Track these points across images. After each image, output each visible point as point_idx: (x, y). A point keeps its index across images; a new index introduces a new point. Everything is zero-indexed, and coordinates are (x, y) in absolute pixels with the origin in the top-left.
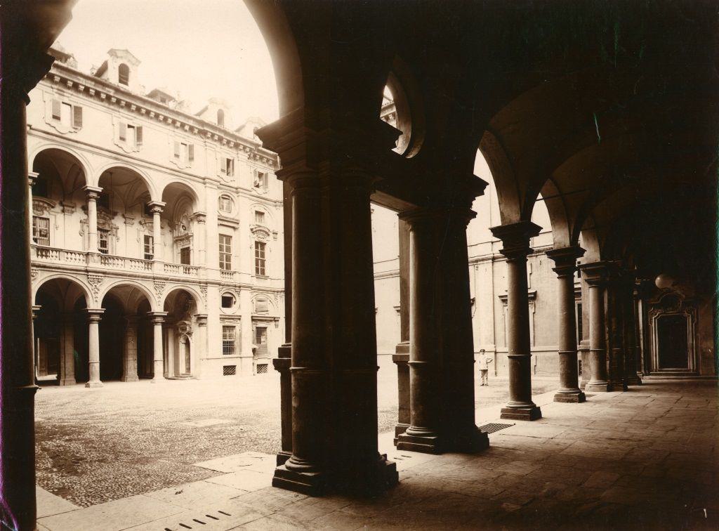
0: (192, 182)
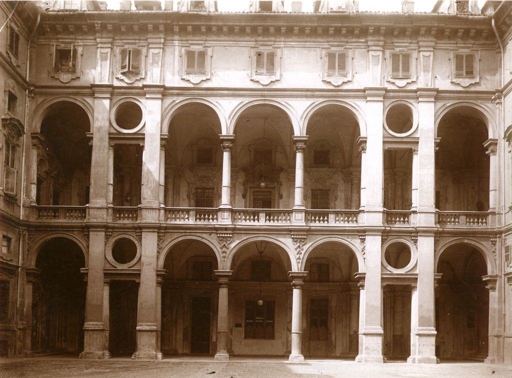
0: (279, 100)
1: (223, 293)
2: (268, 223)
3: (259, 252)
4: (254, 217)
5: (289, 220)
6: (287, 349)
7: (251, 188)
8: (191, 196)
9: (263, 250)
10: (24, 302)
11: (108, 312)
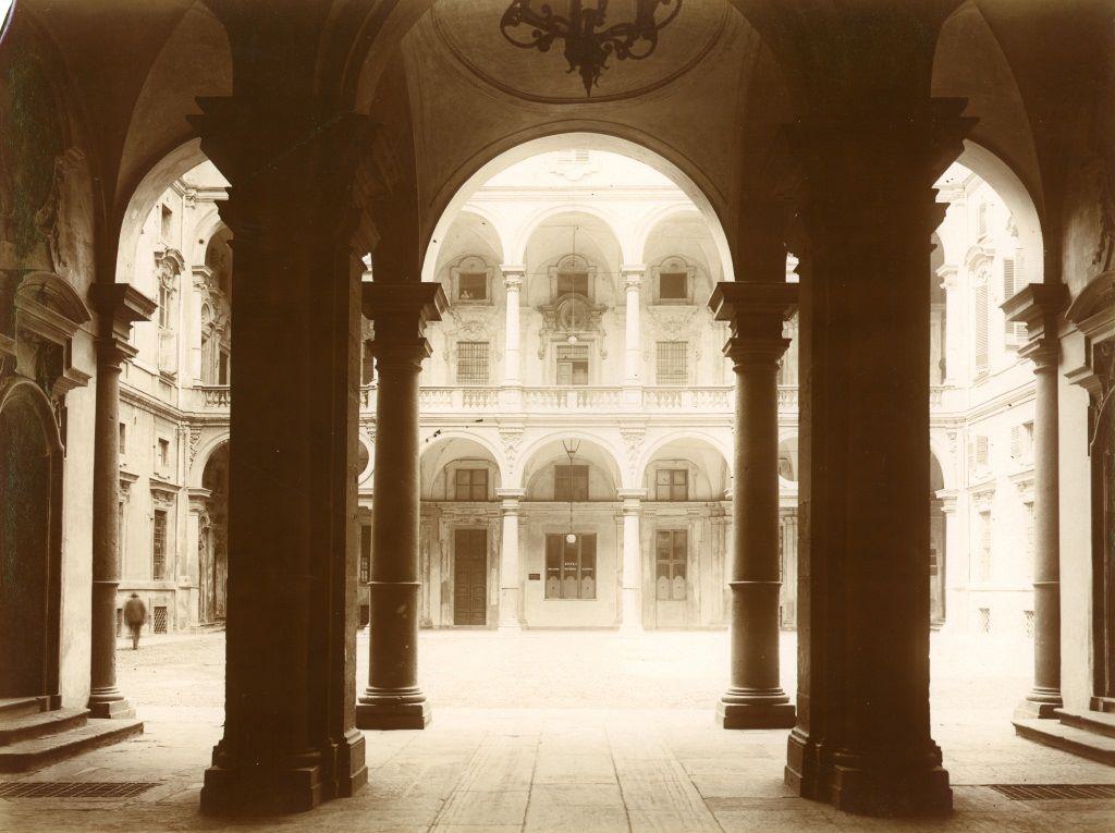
1: (510, 525)
2: (582, 409)
3: (569, 452)
4: (559, 399)
5: (616, 403)
6: (617, 615)
7: (553, 341)
8: (451, 357)
9: (574, 449)
10: (186, 544)
11: (931, 400)
